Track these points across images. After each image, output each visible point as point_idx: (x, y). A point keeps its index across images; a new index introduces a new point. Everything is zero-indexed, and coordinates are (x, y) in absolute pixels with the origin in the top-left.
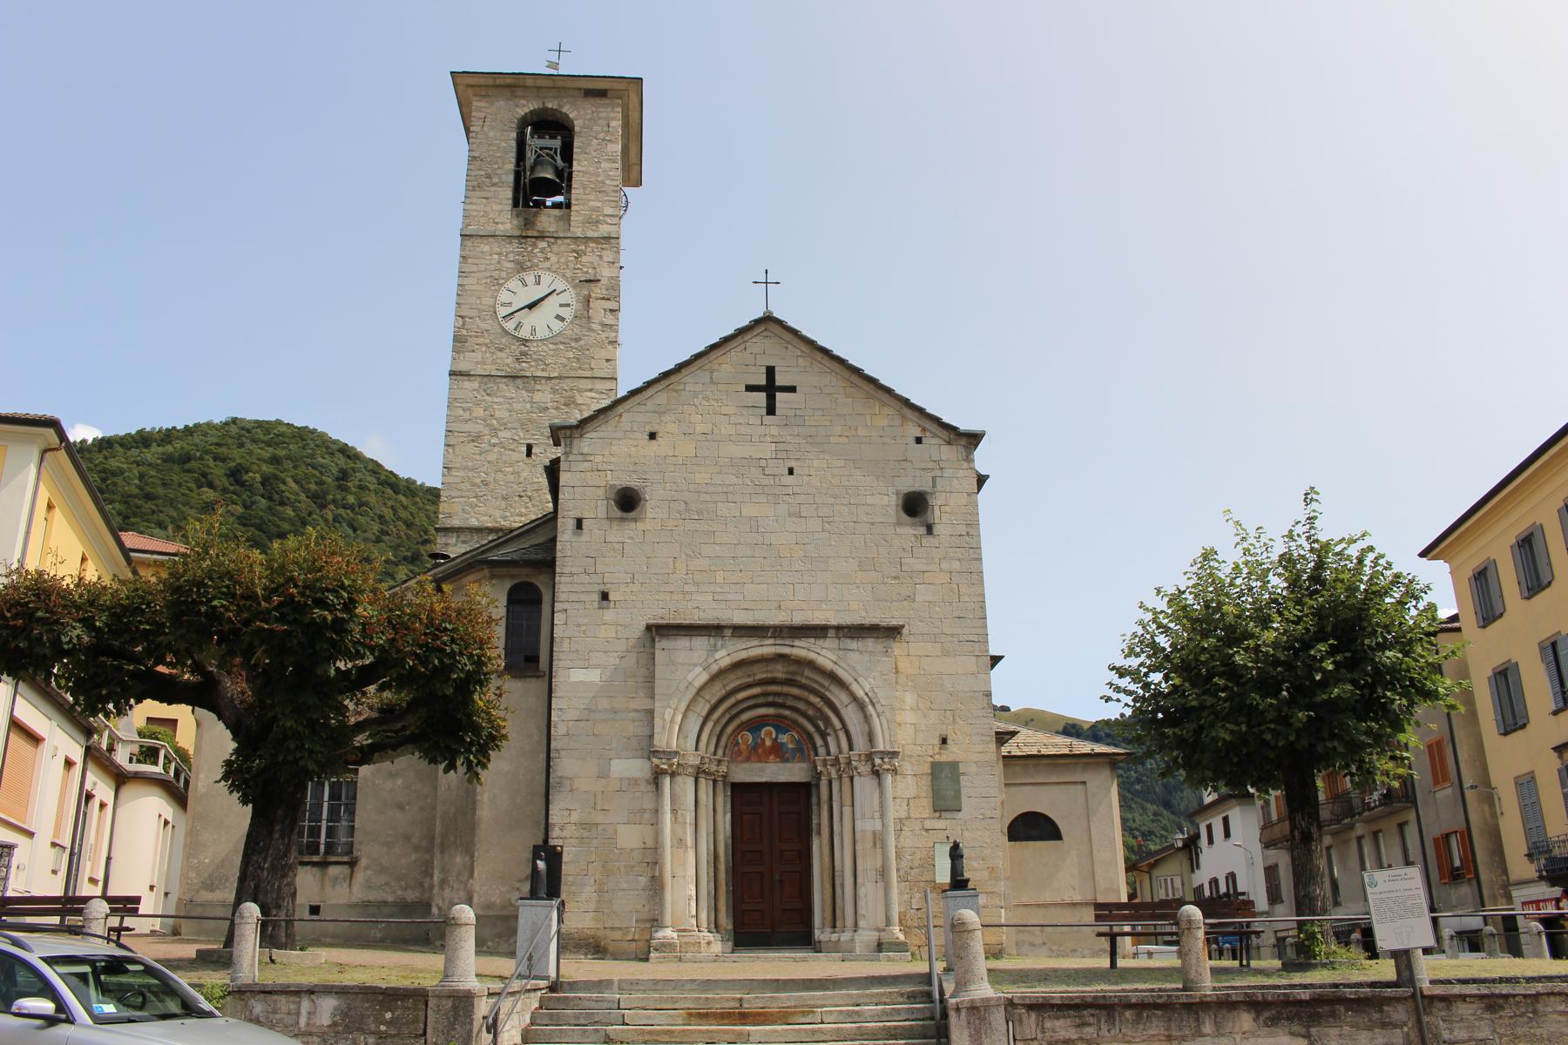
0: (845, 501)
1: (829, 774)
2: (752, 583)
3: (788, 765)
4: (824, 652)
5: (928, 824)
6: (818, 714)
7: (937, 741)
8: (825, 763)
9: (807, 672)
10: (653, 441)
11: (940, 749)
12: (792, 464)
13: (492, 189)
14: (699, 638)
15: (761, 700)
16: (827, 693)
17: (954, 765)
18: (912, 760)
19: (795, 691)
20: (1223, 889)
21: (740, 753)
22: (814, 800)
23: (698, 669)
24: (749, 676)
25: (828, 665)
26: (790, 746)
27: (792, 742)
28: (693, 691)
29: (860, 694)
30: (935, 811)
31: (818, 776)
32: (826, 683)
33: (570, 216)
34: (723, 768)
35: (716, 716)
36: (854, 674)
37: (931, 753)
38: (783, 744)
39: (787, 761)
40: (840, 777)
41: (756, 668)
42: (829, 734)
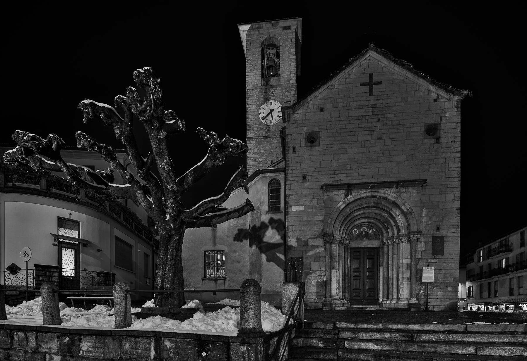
0: (402, 131)
1: (388, 243)
2: (362, 168)
3: (371, 241)
5: (429, 261)
7: (435, 228)
8: (387, 239)
10: (322, 112)
11: (436, 231)
12: (379, 116)
13: (255, 71)
15: (363, 216)
16: (340, 209)
17: (442, 238)
18: (424, 236)
22: (381, 253)
26: (372, 234)
28: (339, 211)
30: (433, 255)
31: (383, 244)
33: (280, 79)
34: (348, 242)
39: (371, 239)
40: (393, 244)
42: (389, 228)
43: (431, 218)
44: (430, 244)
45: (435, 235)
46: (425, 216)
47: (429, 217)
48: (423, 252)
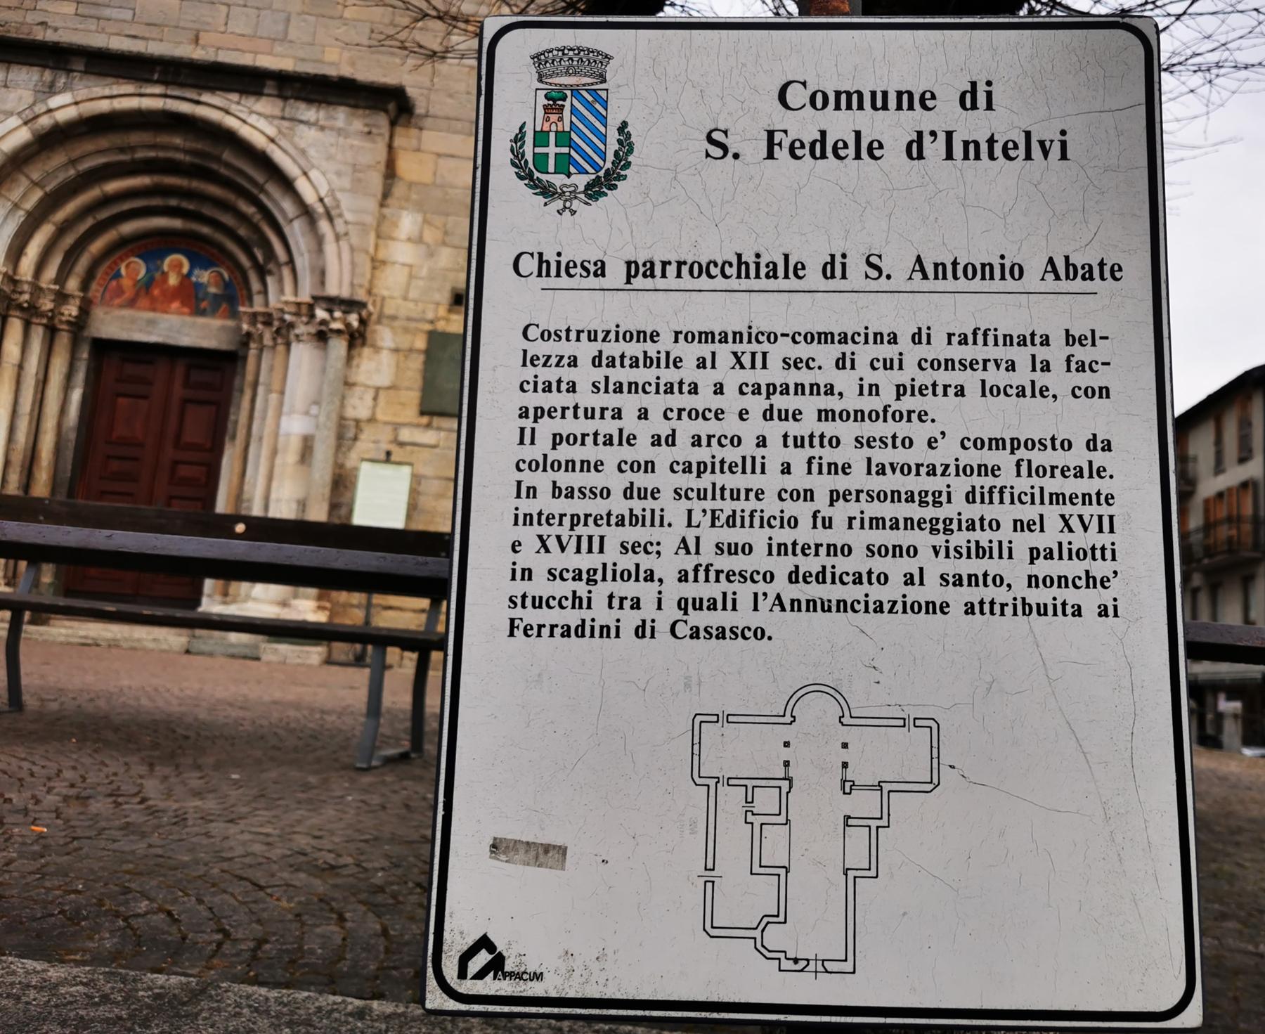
3: (201, 320)
4: (252, 119)
5: (405, 435)
6: (255, 237)
9: (227, 156)
11: (450, 311)
14: (25, 69)
15: (156, 202)
16: (263, 197)
18: (396, 324)
19: (214, 190)
20: (498, 4)
21: (120, 291)
23: (14, 122)
24: (122, 150)
25: (259, 141)
26: (213, 290)
27: (217, 285)
29: (309, 197)
30: (422, 413)
32: (259, 177)
35: (61, 215)
36: (302, 162)
37: (430, 316)
38: (198, 286)
39: (201, 313)
41: (135, 138)
43: (431, 254)
44: (417, 362)
45: (441, 326)
46: (409, 240)
47: (423, 248)
48: (382, 394)
